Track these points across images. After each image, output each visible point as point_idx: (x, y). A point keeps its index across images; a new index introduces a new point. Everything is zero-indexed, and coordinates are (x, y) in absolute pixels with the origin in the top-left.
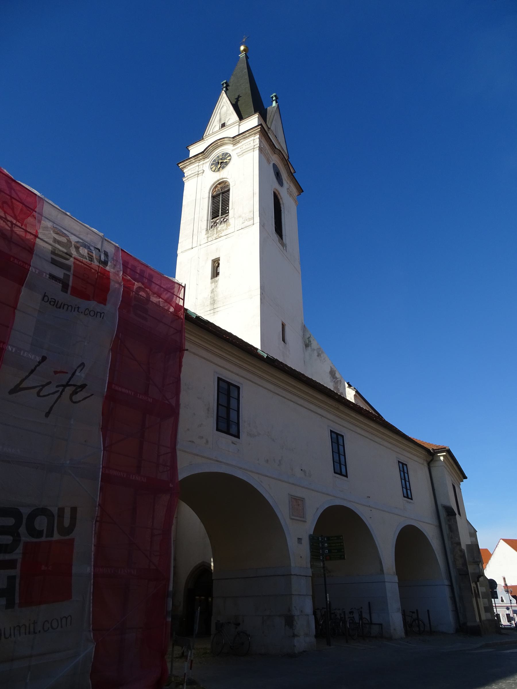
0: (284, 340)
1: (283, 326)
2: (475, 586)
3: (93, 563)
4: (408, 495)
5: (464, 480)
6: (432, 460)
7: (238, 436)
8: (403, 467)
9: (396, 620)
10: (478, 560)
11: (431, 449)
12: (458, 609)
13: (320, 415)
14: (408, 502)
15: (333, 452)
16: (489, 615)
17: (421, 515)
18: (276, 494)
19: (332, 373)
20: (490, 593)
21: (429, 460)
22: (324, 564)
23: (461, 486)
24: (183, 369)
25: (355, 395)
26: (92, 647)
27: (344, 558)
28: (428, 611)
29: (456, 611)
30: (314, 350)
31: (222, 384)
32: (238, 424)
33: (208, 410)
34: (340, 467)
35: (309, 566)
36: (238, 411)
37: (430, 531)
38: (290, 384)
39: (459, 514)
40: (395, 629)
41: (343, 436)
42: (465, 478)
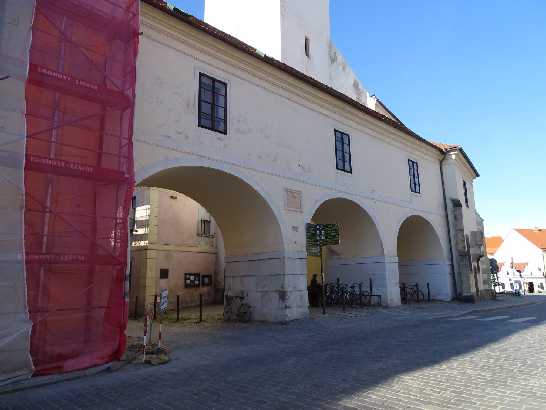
0: (307, 54)
1: (307, 40)
2: (476, 264)
3: (24, 250)
4: (415, 188)
5: (477, 178)
6: (443, 159)
7: (225, 133)
8: (413, 166)
9: (393, 294)
10: (480, 243)
11: (443, 149)
12: (457, 282)
13: (324, 115)
14: (415, 195)
15: (336, 150)
16: (487, 287)
17: (428, 206)
18: (269, 188)
19: (356, 85)
20: (490, 270)
21: (441, 159)
22: (321, 248)
23: (473, 184)
24: (139, 56)
25: (376, 104)
26: (28, 327)
27: (338, 243)
28: (428, 284)
29: (454, 284)
30: (339, 64)
31: (338, 134)
32: (225, 121)
33: (188, 105)
34: (343, 163)
35: (305, 250)
36: (226, 108)
37: (437, 221)
38: (289, 83)
39: (467, 205)
40: (391, 300)
41: (348, 136)
42: (478, 175)
